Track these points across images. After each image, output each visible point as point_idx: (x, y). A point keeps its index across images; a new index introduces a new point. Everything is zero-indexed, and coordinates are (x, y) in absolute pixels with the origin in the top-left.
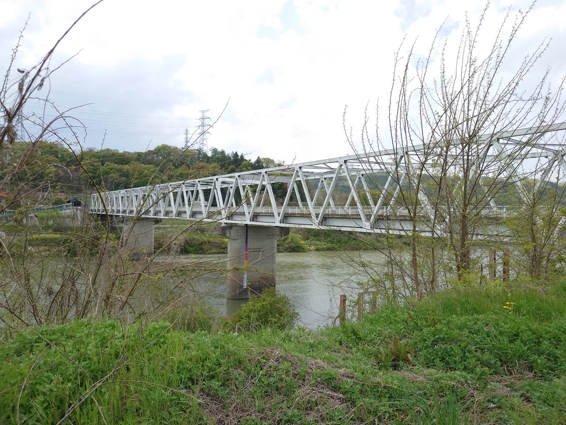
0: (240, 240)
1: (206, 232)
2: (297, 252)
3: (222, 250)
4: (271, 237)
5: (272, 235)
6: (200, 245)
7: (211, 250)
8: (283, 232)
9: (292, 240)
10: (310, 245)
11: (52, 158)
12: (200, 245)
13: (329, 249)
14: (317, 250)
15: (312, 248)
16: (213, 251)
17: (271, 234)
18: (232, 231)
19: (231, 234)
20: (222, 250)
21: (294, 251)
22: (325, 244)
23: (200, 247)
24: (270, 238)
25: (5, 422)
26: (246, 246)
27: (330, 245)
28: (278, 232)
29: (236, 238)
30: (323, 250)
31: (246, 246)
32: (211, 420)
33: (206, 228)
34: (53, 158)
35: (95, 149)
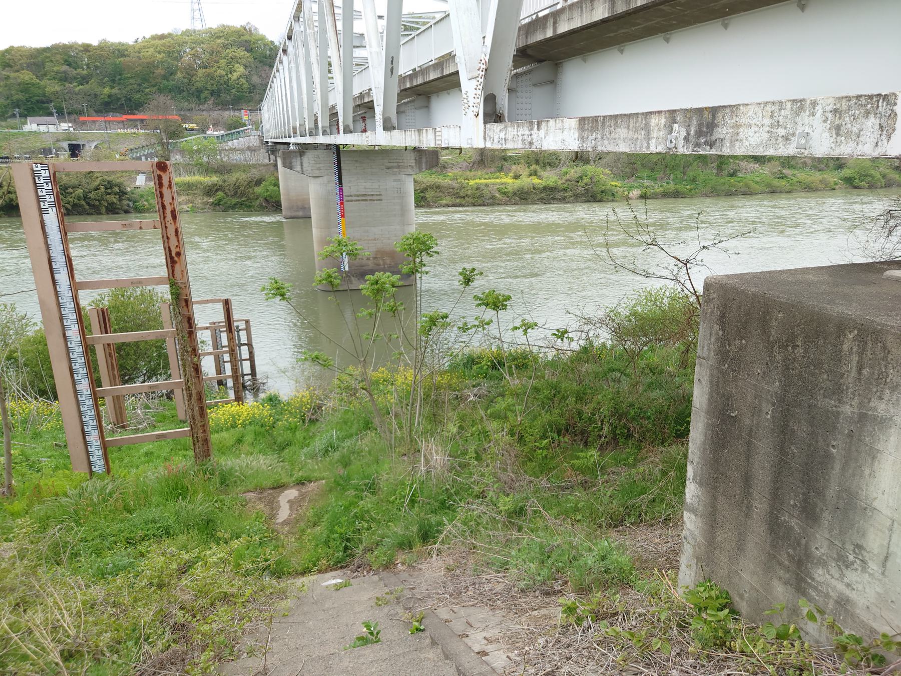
0: (325, 179)
1: (449, 170)
2: (600, 201)
3: (458, 201)
4: (395, 170)
5: (399, 167)
6: (422, 192)
7: (441, 200)
8: (424, 160)
9: (591, 179)
10: (630, 188)
11: (241, 52)
12: (422, 192)
13: (666, 195)
14: (643, 197)
15: (636, 193)
16: (444, 202)
17: (395, 164)
18: (305, 160)
19: (305, 165)
20: (458, 201)
21: (595, 201)
22: (661, 186)
23: (422, 194)
24: (395, 173)
25: (256, 439)
26: (341, 189)
27: (672, 187)
28: (411, 159)
29: (317, 173)
30: (655, 196)
31: (341, 189)
32: (4, 565)
33: (450, 162)
34: (242, 53)
35: (256, 29)
